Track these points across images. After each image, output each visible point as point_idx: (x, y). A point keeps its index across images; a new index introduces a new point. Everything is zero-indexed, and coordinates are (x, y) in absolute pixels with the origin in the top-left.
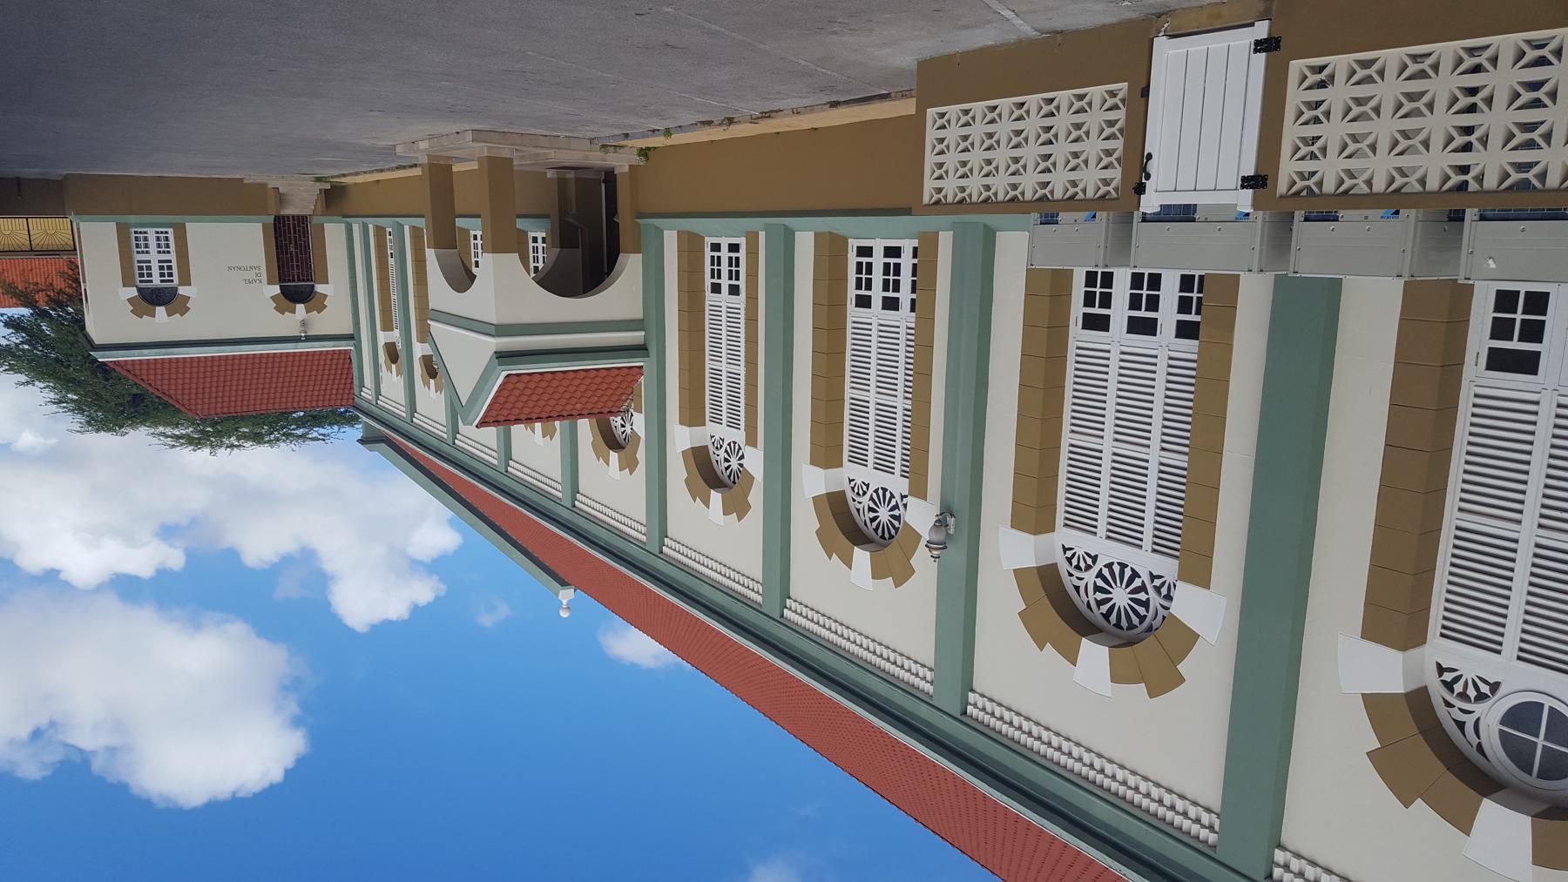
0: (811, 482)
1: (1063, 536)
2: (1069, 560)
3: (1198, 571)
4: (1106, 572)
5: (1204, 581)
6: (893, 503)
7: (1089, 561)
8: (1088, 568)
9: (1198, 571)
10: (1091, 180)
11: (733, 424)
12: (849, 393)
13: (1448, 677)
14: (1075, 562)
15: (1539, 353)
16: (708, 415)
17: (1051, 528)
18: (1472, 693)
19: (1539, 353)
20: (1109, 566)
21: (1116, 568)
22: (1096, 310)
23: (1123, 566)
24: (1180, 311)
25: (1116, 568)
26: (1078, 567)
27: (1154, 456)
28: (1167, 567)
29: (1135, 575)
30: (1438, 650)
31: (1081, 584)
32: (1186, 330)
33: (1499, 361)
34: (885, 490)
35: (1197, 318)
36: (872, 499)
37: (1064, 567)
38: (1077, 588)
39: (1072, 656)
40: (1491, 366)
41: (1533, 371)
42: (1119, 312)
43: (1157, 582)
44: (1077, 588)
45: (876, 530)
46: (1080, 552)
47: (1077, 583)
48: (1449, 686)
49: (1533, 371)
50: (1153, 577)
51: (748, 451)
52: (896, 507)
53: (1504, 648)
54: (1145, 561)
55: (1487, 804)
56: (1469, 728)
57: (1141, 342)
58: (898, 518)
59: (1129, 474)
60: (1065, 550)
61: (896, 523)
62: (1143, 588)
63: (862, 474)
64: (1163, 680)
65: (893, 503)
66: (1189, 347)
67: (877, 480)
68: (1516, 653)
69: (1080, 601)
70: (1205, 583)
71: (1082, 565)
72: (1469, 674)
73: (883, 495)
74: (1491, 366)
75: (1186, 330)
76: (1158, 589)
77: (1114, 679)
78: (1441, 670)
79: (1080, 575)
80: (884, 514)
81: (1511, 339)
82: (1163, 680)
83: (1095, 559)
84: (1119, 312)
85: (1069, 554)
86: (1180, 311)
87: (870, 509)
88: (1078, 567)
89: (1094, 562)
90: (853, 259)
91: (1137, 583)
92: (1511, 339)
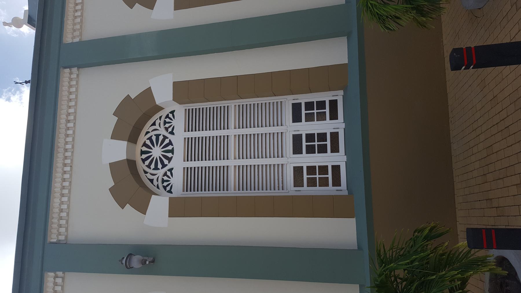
3: (178, 208)
4: (167, 141)
7: (170, 130)
9: (178, 208)
12: (233, 104)
13: (171, 116)
18: (165, 184)
20: (170, 143)
23: (172, 151)
29: (170, 159)
30: (180, 111)
31: (157, 127)
33: (296, 107)
37: (163, 113)
40: (294, 105)
41: (294, 121)
42: (305, 128)
43: (169, 173)
44: (154, 124)
46: (174, 123)
48: (167, 116)
49: (294, 121)
50: (171, 170)
53: (187, 133)
56: (154, 127)
59: (219, 147)
62: (164, 166)
63: (179, 122)
68: (187, 137)
69: (147, 127)
72: (172, 181)
74: (294, 105)
76: (165, 174)
77: (111, 165)
78: (172, 112)
81: (306, 142)
83: (172, 133)
84: (305, 128)
85: (171, 116)
90: (326, 97)
91: (166, 162)
92: (306, 142)
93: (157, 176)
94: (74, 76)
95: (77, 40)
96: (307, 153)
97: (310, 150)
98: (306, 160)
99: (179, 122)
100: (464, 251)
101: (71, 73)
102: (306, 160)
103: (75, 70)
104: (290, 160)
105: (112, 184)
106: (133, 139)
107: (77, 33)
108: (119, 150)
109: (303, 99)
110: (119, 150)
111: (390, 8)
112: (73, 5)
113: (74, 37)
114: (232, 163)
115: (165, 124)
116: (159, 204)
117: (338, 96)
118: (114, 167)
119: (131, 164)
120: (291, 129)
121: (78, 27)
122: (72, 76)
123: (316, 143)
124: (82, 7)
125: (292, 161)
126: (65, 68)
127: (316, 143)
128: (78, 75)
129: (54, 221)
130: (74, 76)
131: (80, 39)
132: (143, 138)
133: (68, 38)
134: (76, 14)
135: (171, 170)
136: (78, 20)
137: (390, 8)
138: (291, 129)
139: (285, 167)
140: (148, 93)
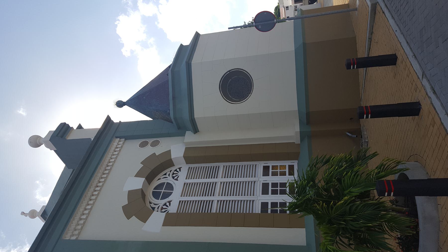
1: (185, 168)
2: (176, 170)
3: (171, 220)
5: (166, 224)
7: (176, 178)
8: (173, 177)
9: (171, 220)
12: (221, 165)
14: (175, 172)
15: (272, 183)
17: (187, 163)
19: (272, 183)
22: (270, 188)
24: (272, 203)
31: (167, 176)
32: (264, 205)
33: (266, 169)
35: (269, 211)
37: (173, 169)
38: (165, 174)
39: (138, 175)
42: (271, 179)
43: (168, 204)
44: (165, 174)
46: (179, 174)
47: (167, 174)
50: (170, 202)
54: (176, 197)
55: (143, 179)
56: (165, 176)
57: (259, 188)
64: (128, 211)
66: (258, 209)
67: (178, 186)
70: (165, 224)
71: (174, 175)
75: (264, 205)
76: (165, 204)
79: (171, 175)
82: (128, 211)
84: (271, 179)
86: (272, 203)
88: (173, 174)
89: (175, 179)
93: (158, 206)
94: (121, 143)
95: (74, 238)
96: (272, 194)
97: (274, 192)
98: (270, 198)
99: (183, 175)
100: (389, 246)
101: (120, 141)
102: (270, 198)
103: (124, 139)
104: (259, 198)
105: (126, 203)
106: (149, 179)
107: (77, 232)
108: (138, 183)
109: (270, 164)
110: (138, 183)
111: (324, 210)
112: (83, 210)
113: (73, 235)
114: (216, 198)
115: (173, 175)
116: (157, 218)
117: (295, 164)
118: (131, 193)
119: (142, 193)
120: (261, 179)
121: (79, 227)
122: (120, 143)
123: (278, 189)
124: (89, 212)
125: (260, 198)
126: (117, 137)
127: (278, 189)
128: (123, 143)
129: (73, 225)
130: (121, 143)
131: (77, 238)
132: (156, 183)
133: (68, 236)
134: (111, 160)
135: (170, 202)
136: (113, 160)
137: (324, 210)
138: (261, 179)
139: (255, 202)
140: (169, 153)
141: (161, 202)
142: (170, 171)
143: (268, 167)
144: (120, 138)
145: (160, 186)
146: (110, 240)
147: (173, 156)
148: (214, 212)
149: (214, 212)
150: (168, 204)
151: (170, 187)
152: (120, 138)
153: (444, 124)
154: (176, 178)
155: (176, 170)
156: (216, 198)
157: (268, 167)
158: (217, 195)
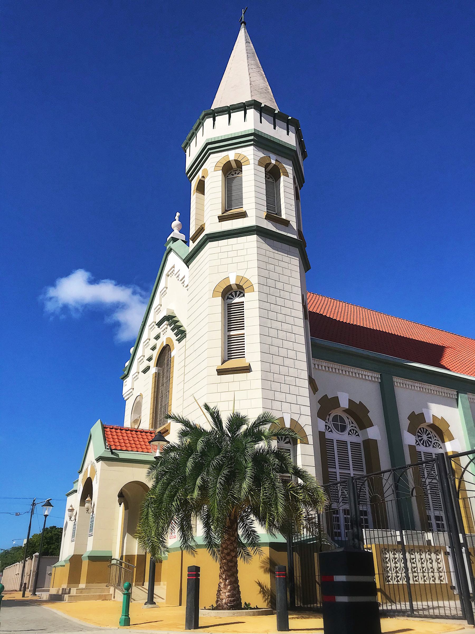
0: (375, 432)
2: (356, 432)
6: (422, 442)
7: (350, 433)
8: (350, 431)
10: (390, 555)
11: (342, 443)
14: (355, 432)
16: (362, 447)
21: (428, 445)
25: (428, 445)
26: (353, 430)
27: (428, 481)
28: (328, 435)
31: (351, 425)
34: (426, 446)
36: (431, 442)
37: (358, 429)
38: (352, 423)
44: (352, 423)
45: (427, 430)
46: (354, 436)
50: (331, 431)
51: (413, 443)
52: (420, 440)
58: (419, 436)
60: (358, 435)
61: (419, 434)
65: (422, 442)
67: (345, 437)
71: (352, 431)
73: (427, 444)
79: (352, 428)
80: (425, 437)
87: (430, 438)
88: (353, 430)
101: (378, 378)
103: (380, 381)
114: (338, 471)
135: (331, 431)
140: (371, 425)
141: (331, 424)
142: (355, 427)
143: (366, 515)
144: (381, 378)
145: (342, 420)
146: (323, 624)
147: (369, 430)
148: (329, 470)
149: (329, 470)
150: (330, 430)
151: (343, 429)
152: (381, 378)
153: (100, 602)
154: (350, 433)
155: (356, 432)
156: (338, 471)
157: (366, 515)
158: (340, 471)
